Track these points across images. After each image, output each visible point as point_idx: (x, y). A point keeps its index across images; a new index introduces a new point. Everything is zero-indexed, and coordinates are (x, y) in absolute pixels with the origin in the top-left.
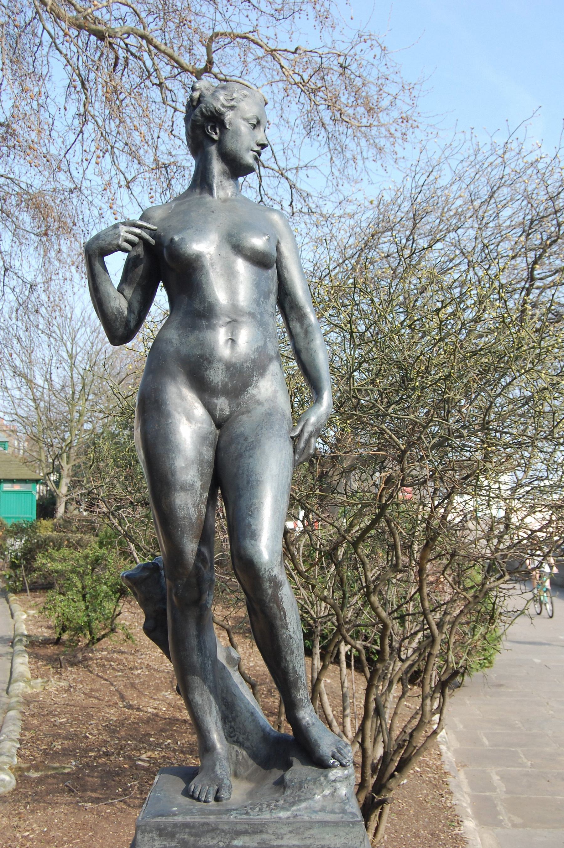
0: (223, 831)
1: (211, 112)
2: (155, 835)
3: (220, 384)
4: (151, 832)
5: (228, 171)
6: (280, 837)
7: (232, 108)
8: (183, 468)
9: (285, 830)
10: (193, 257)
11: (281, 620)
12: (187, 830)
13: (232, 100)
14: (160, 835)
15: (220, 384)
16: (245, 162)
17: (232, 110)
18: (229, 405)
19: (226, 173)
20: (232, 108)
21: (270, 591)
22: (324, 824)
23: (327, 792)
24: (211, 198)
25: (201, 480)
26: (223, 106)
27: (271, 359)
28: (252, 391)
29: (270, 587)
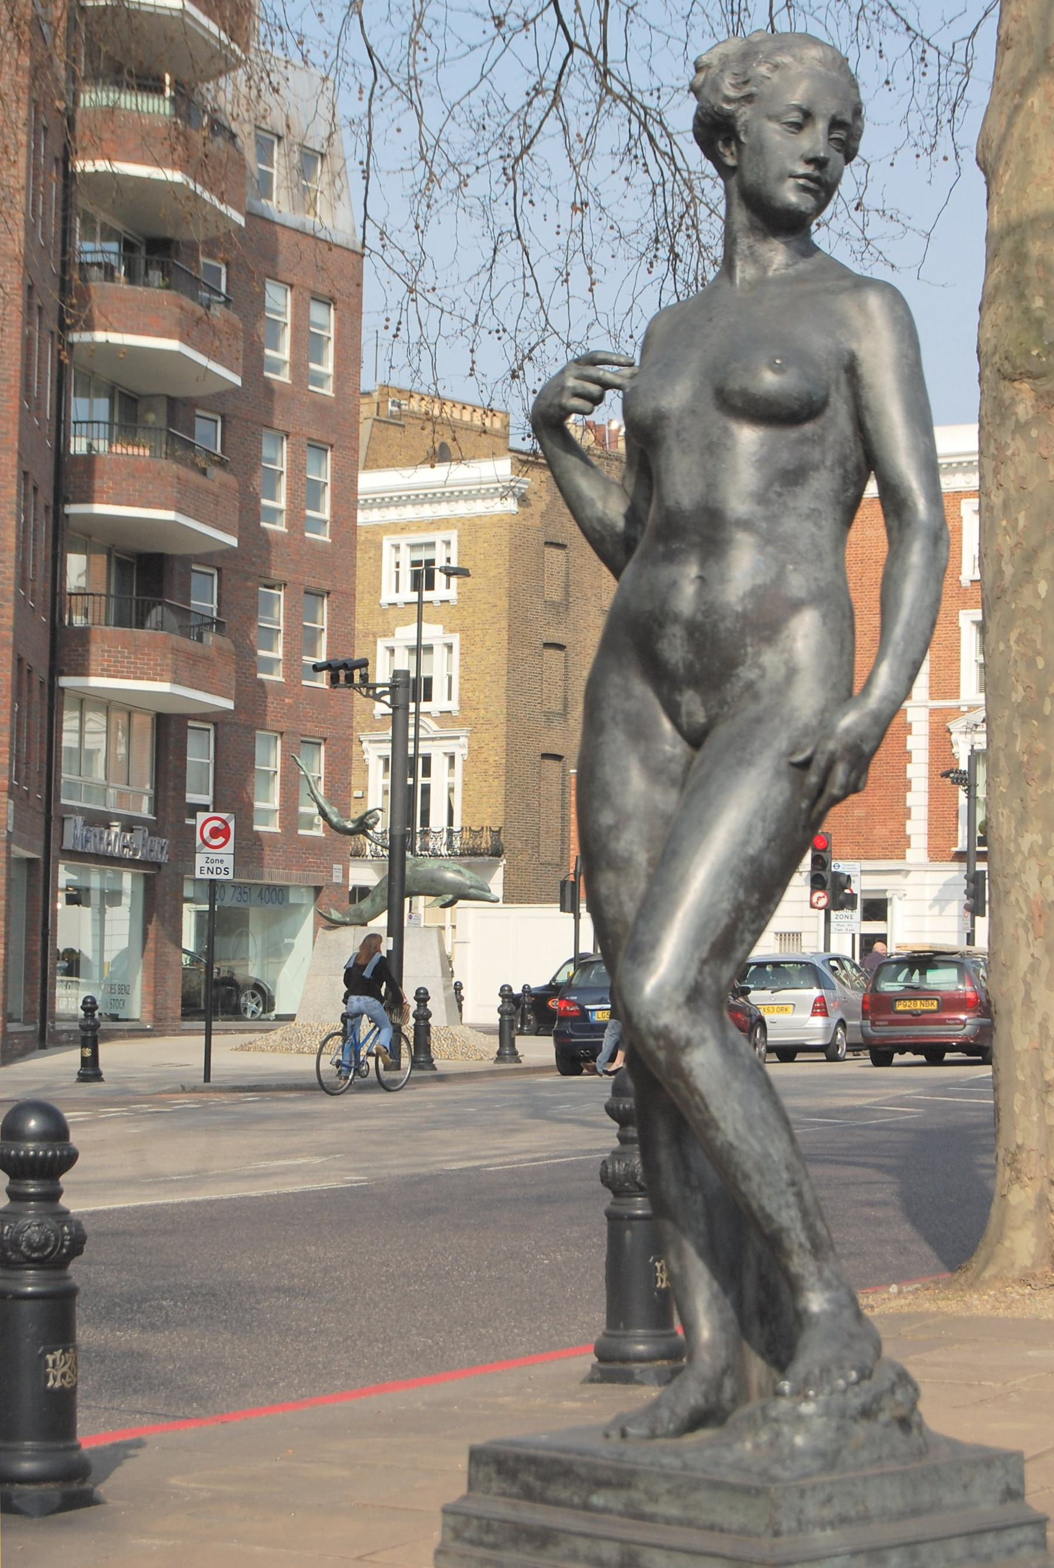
0: (578, 1476)
1: (710, 116)
2: (492, 1470)
3: (681, 665)
4: (487, 1464)
5: (760, 224)
6: (653, 1498)
7: (749, 98)
8: (610, 828)
9: (661, 1487)
10: (648, 422)
11: (700, 1111)
12: (533, 1468)
13: (746, 83)
14: (499, 1472)
15: (681, 665)
16: (778, 204)
17: (750, 102)
18: (704, 704)
19: (757, 228)
20: (749, 98)
21: (661, 1055)
22: (716, 1486)
23: (764, 1437)
24: (728, 285)
25: (648, 851)
26: (728, 100)
27: (796, 606)
28: (747, 673)
29: (659, 1048)
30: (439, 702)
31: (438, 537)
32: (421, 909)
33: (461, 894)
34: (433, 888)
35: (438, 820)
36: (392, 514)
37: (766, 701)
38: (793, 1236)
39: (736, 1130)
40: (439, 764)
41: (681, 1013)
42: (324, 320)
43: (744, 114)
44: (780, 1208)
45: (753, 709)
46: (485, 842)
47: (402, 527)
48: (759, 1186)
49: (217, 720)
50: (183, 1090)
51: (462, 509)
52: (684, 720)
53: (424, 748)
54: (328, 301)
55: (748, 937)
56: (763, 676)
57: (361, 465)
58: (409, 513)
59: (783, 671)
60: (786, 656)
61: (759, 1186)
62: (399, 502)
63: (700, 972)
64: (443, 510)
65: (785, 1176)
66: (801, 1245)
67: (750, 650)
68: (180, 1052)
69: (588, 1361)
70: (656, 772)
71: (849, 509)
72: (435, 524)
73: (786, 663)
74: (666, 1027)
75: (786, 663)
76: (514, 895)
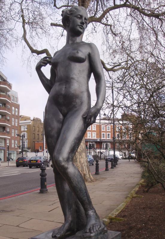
8: (50, 130)
30: (26, 138)
31: (25, 126)
32: (24, 153)
33: (27, 151)
34: (25, 151)
35: (26, 146)
36: (22, 124)
37: (77, 108)
38: (86, 201)
39: (76, 184)
40: (26, 142)
41: (66, 163)
42: (17, 109)
43: (71, 17)
44: (83, 197)
45: (75, 109)
46: (29, 148)
47: (22, 125)
48: (80, 193)
49: (9, 139)
50: (7, 166)
51: (27, 124)
52: (63, 112)
53: (25, 141)
54: (17, 108)
55: (77, 148)
56: (77, 104)
57: (20, 120)
58: (23, 124)
59: (80, 103)
60: (80, 100)
61: (80, 193)
62: (22, 124)
63: (69, 155)
64: (26, 124)
65: (84, 191)
66: (87, 203)
67: (74, 99)
68: (6, 164)
69: (39, 191)
70: (58, 121)
71: (89, 77)
72: (25, 125)
73: (81, 101)
74: (63, 165)
75: (81, 101)
76: (31, 152)
